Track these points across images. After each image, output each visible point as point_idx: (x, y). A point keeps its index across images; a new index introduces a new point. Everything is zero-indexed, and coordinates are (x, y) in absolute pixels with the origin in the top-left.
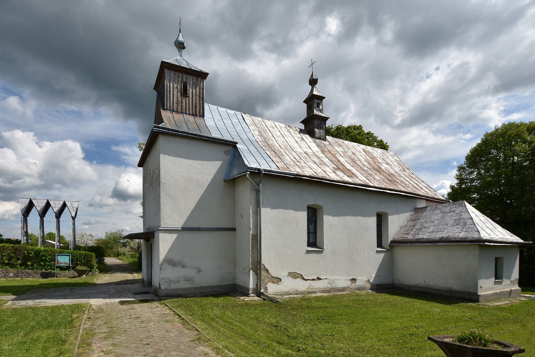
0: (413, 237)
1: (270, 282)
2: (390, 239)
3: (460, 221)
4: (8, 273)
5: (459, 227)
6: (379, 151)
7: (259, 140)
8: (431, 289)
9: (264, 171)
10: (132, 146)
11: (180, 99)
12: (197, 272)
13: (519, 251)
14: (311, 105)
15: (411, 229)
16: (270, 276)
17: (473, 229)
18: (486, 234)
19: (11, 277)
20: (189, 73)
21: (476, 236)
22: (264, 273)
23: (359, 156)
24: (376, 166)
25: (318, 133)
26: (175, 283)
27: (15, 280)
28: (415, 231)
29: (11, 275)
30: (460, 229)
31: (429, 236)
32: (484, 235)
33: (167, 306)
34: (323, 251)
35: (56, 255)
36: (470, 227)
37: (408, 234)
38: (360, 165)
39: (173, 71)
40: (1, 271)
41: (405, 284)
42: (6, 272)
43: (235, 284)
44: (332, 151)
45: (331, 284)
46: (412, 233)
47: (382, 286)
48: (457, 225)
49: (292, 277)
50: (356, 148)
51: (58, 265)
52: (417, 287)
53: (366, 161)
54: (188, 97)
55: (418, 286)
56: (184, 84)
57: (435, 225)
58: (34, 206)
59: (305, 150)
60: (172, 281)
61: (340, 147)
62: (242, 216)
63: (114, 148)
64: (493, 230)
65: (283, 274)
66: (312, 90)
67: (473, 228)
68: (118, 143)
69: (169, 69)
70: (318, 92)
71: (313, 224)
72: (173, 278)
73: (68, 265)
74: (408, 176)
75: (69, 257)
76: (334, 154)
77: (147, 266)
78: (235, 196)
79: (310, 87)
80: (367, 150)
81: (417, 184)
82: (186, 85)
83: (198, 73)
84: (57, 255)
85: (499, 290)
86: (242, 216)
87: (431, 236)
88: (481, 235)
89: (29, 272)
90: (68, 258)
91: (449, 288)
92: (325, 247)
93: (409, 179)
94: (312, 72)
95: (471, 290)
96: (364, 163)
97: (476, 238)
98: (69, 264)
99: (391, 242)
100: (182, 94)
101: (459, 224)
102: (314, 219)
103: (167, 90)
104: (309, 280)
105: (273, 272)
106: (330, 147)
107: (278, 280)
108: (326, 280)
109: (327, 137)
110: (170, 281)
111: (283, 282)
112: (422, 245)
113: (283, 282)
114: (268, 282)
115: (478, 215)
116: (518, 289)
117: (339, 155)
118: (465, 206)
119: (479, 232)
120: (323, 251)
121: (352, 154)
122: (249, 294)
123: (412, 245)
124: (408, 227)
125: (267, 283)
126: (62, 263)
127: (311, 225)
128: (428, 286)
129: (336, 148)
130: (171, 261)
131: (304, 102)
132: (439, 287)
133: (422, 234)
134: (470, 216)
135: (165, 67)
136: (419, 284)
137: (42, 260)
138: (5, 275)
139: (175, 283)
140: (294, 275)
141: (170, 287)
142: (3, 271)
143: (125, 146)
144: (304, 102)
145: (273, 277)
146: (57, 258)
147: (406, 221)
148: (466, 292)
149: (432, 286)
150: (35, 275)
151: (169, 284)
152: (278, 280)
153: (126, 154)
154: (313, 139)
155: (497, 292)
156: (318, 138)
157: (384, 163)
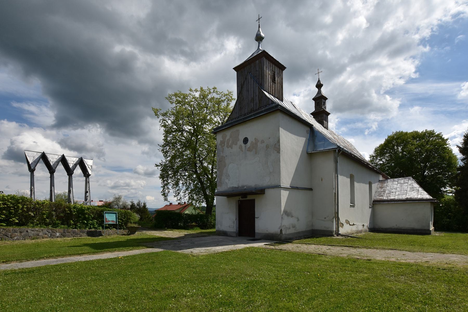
4: (54, 232)
10: (41, 105)
11: (271, 84)
19: (58, 237)
27: (82, 238)
29: (58, 234)
31: (398, 197)
34: (354, 206)
35: (104, 213)
40: (47, 231)
42: (52, 232)
43: (313, 230)
51: (107, 223)
52: (391, 229)
54: (276, 83)
62: (322, 180)
63: (15, 105)
66: (319, 92)
68: (20, 100)
73: (115, 223)
75: (115, 215)
77: (236, 219)
84: (105, 213)
86: (322, 180)
89: (75, 231)
90: (115, 216)
94: (319, 79)
95: (426, 228)
98: (116, 222)
101: (414, 190)
103: (265, 75)
112: (396, 202)
120: (354, 206)
123: (389, 203)
126: (109, 221)
128: (399, 228)
131: (313, 99)
137: (85, 218)
138: (51, 235)
142: (49, 231)
143: (29, 104)
144: (313, 99)
146: (105, 216)
149: (401, 228)
150: (81, 234)
153: (32, 113)
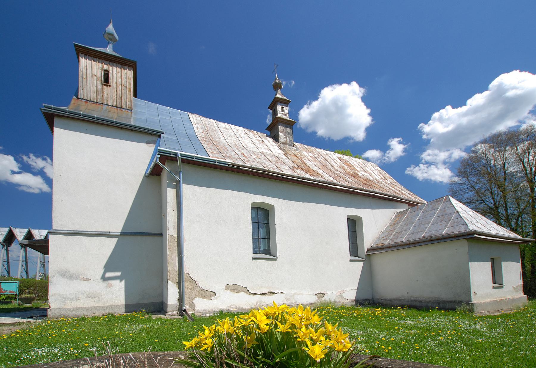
0: (391, 241)
1: (198, 296)
2: (367, 246)
3: (444, 217)
5: (443, 223)
6: (357, 161)
7: (211, 144)
8: (415, 301)
9: (181, 156)
12: (106, 287)
13: (519, 251)
14: (275, 109)
15: (390, 234)
16: (199, 289)
17: (460, 223)
18: (476, 228)
20: (112, 60)
21: (462, 230)
22: (189, 285)
23: (333, 163)
24: (352, 173)
25: (283, 138)
26: (72, 300)
28: (394, 236)
30: (444, 225)
32: (472, 227)
33: (352, 345)
36: (456, 222)
37: (386, 239)
38: (332, 169)
39: (91, 56)
41: (386, 298)
44: (298, 155)
45: (289, 299)
46: (391, 238)
47: (359, 302)
48: (440, 221)
49: (232, 290)
50: (330, 156)
52: (400, 300)
53: (340, 167)
55: (401, 298)
56: (105, 72)
57: (416, 225)
58: (16, 239)
59: (261, 150)
60: (68, 298)
61: (310, 153)
64: (485, 225)
65: (218, 287)
67: (459, 222)
69: (85, 54)
70: (283, 94)
71: (265, 228)
72: (70, 294)
74: (389, 184)
76: (301, 157)
78: (161, 195)
79: (275, 91)
80: (343, 158)
81: (399, 191)
82: (108, 73)
83: (123, 61)
85: (499, 297)
87: (412, 237)
88: (469, 227)
91: (436, 298)
92: (278, 254)
93: (390, 186)
96: (337, 168)
97: (463, 232)
99: (368, 250)
100: (102, 82)
101: (442, 221)
102: (266, 222)
104: (258, 294)
105: (203, 285)
106: (297, 152)
107: (210, 294)
108: (282, 294)
109: (295, 143)
110: (65, 298)
111: (218, 297)
113: (218, 297)
114: (195, 296)
115: (467, 210)
116: (524, 297)
117: (306, 159)
118: (450, 201)
119: (466, 224)
121: (323, 160)
122: (166, 312)
124: (387, 232)
125: (195, 298)
126: (6, 291)
127: (262, 229)
128: (412, 299)
129: (305, 153)
130: (66, 272)
132: (424, 299)
133: (401, 238)
134: (456, 210)
135: (80, 51)
136: (402, 297)
139: (72, 300)
140: (235, 289)
141: (65, 305)
145: (203, 290)
147: (385, 227)
148: (456, 301)
149: (416, 298)
151: (63, 302)
152: (210, 294)
154: (277, 143)
155: (496, 300)
156: (282, 143)
157: (362, 171)
